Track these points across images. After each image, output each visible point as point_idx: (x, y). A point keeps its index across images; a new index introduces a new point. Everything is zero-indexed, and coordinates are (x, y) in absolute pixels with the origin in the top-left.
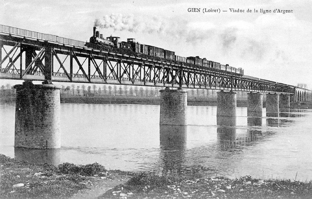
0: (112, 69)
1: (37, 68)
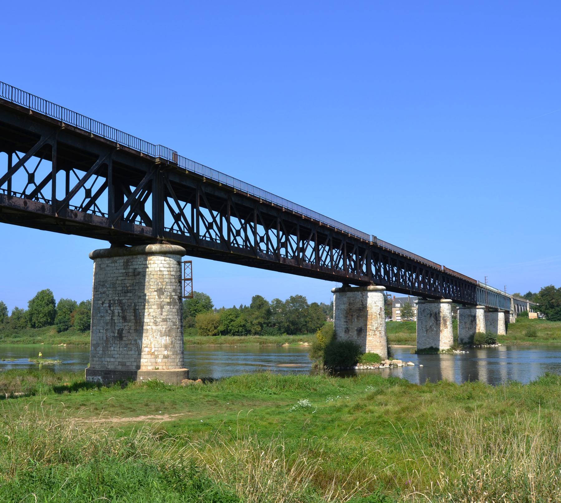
0: (177, 211)
1: (135, 217)
